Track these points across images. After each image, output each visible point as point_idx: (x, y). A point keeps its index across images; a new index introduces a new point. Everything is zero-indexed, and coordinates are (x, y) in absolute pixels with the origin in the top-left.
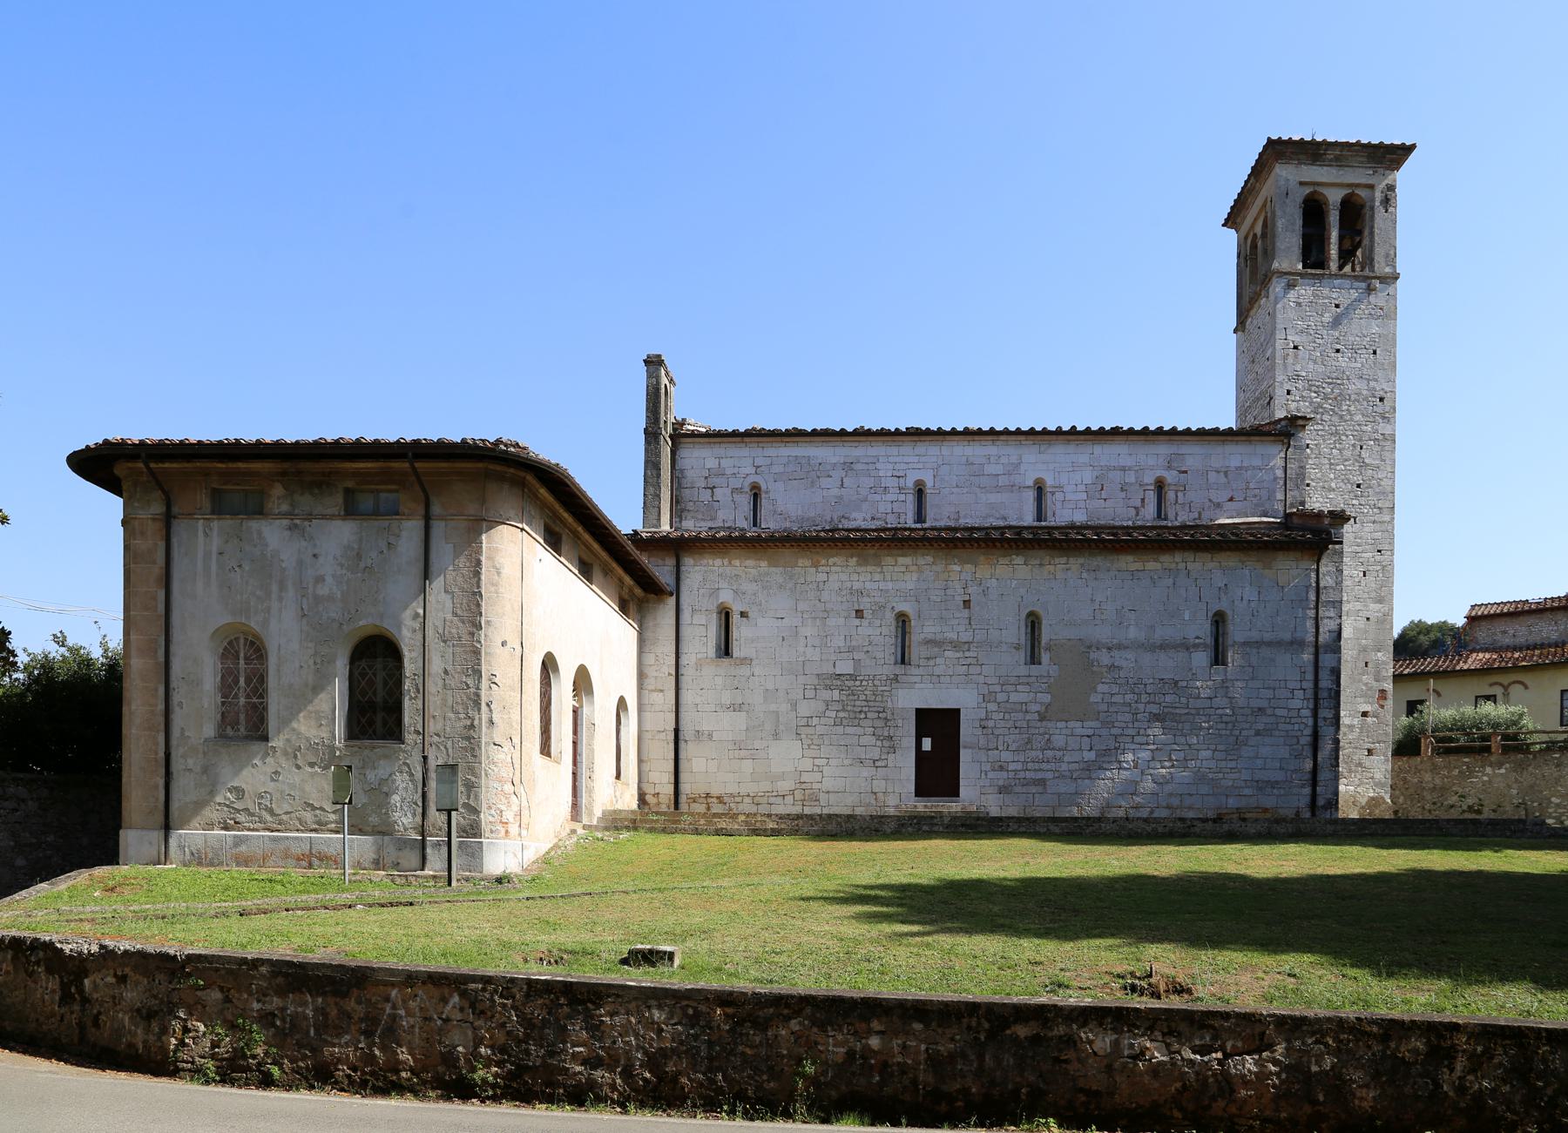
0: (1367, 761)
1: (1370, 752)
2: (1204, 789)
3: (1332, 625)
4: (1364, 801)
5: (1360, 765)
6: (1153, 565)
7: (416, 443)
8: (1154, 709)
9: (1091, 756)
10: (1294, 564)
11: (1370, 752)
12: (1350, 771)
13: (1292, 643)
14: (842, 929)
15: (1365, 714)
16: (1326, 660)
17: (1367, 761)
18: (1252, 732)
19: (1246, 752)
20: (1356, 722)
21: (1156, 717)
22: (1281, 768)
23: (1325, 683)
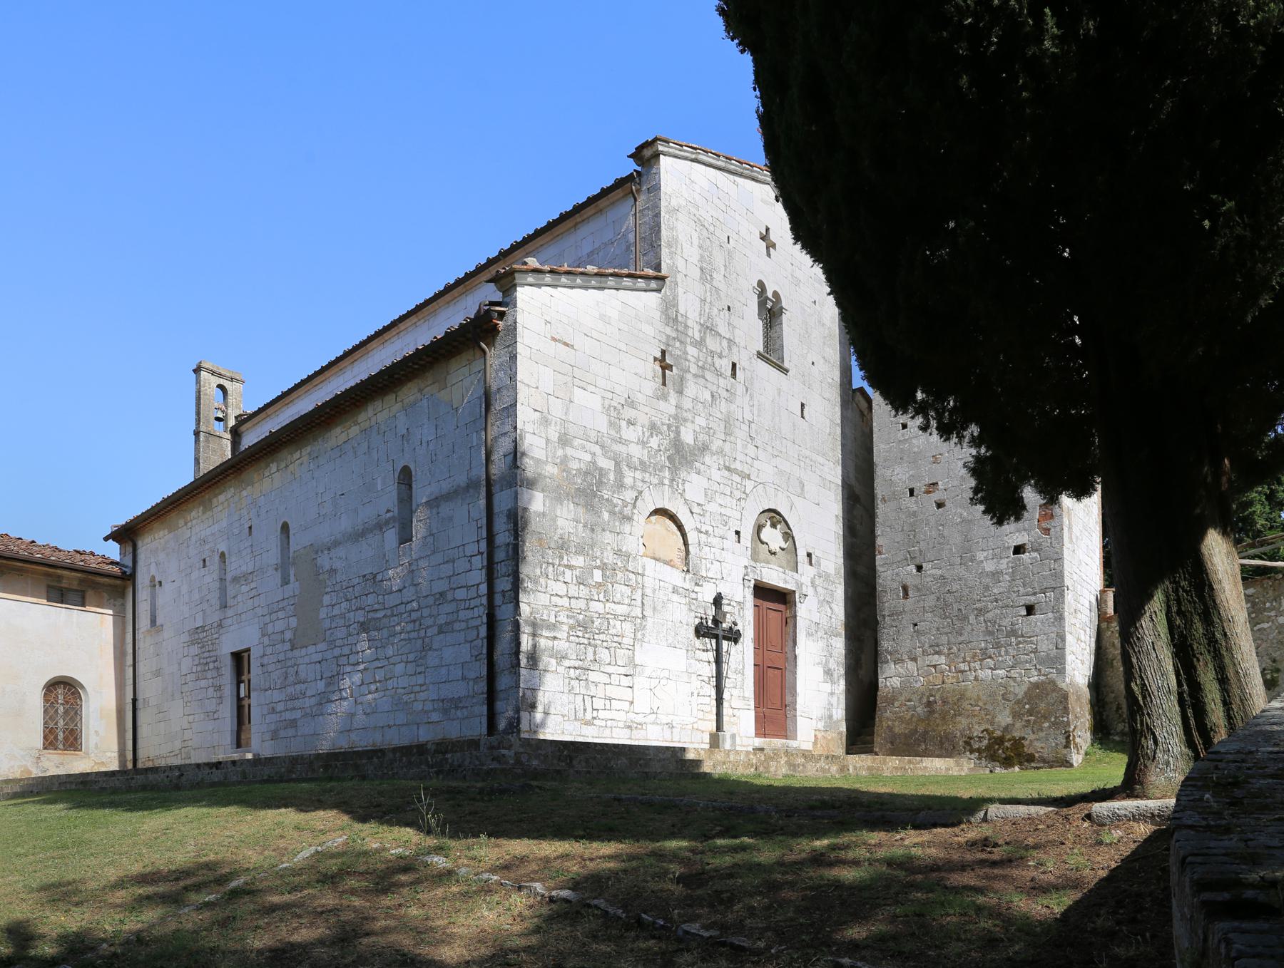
0: (1024, 624)
1: (1030, 610)
2: (401, 718)
3: (504, 445)
4: (1020, 691)
5: (1013, 633)
6: (338, 435)
7: (164, 500)
8: (360, 616)
9: (321, 685)
10: (465, 370)
11: (1030, 610)
12: (998, 646)
13: (468, 486)
14: (143, 918)
15: (1019, 550)
16: (502, 502)
17: (1024, 624)
18: (435, 630)
19: (432, 659)
20: (1004, 564)
21: (364, 627)
22: (464, 678)
23: (502, 538)
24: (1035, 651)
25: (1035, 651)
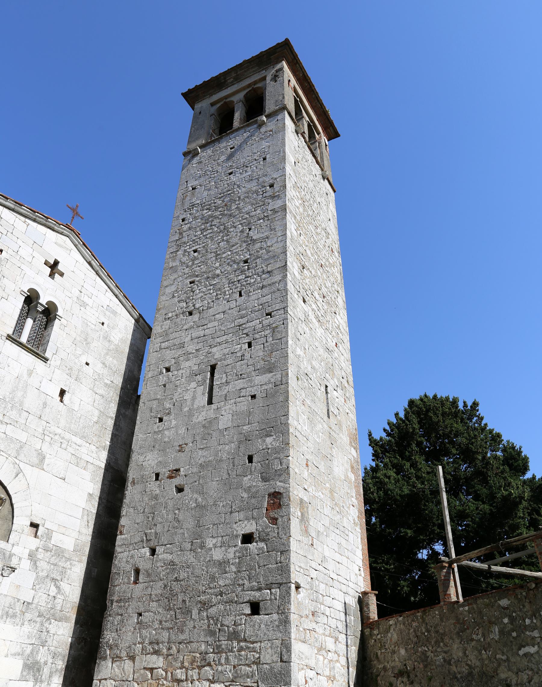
1: (255, 608)
5: (234, 636)
11: (255, 608)
15: (248, 539)
24: (257, 662)
25: (257, 662)
